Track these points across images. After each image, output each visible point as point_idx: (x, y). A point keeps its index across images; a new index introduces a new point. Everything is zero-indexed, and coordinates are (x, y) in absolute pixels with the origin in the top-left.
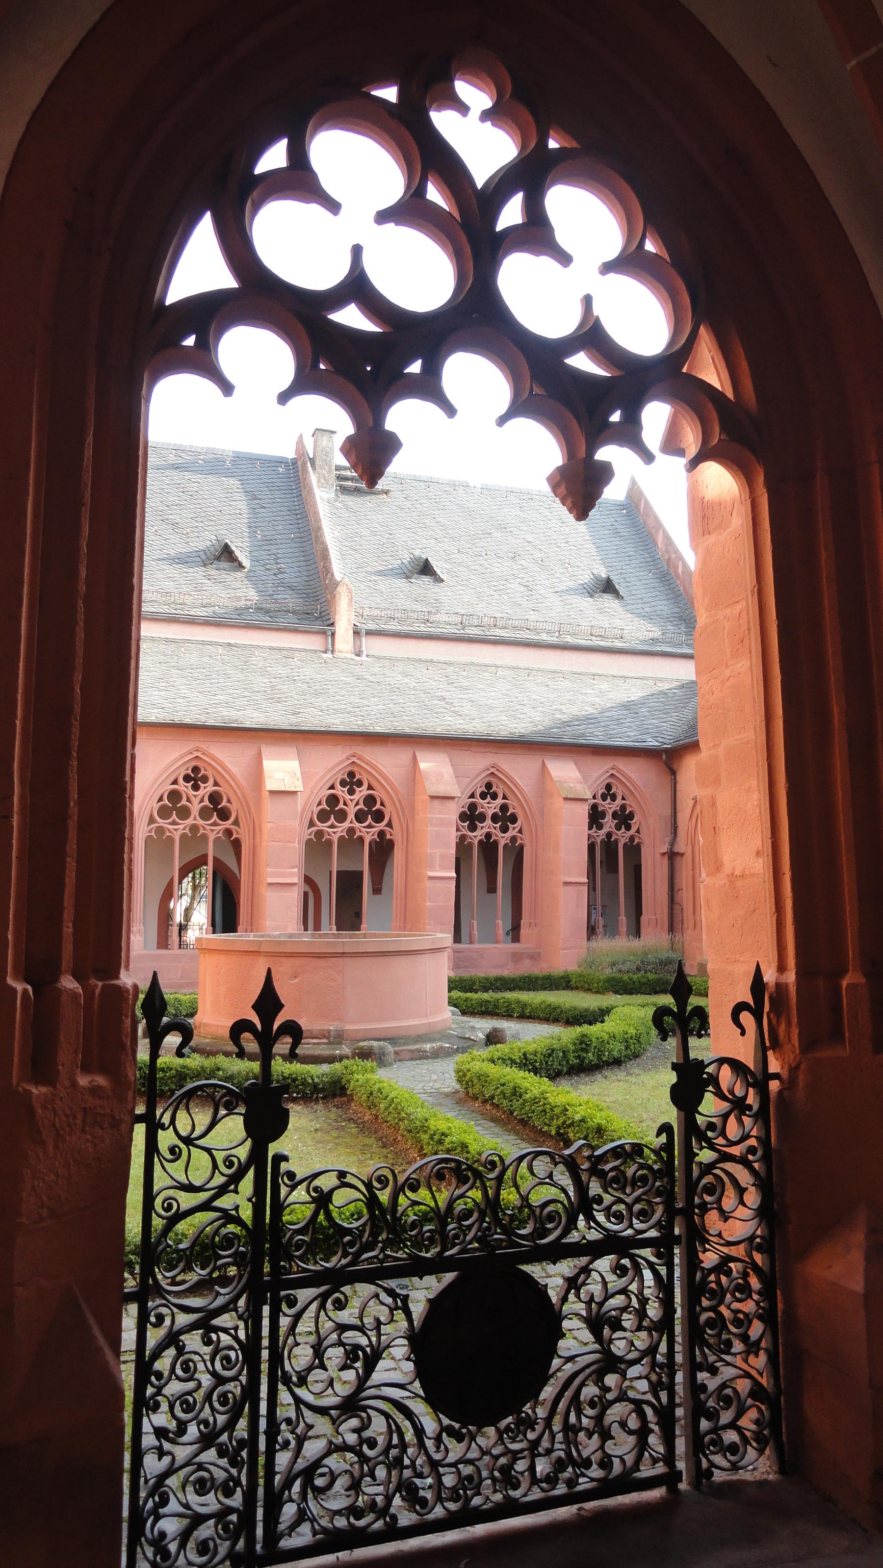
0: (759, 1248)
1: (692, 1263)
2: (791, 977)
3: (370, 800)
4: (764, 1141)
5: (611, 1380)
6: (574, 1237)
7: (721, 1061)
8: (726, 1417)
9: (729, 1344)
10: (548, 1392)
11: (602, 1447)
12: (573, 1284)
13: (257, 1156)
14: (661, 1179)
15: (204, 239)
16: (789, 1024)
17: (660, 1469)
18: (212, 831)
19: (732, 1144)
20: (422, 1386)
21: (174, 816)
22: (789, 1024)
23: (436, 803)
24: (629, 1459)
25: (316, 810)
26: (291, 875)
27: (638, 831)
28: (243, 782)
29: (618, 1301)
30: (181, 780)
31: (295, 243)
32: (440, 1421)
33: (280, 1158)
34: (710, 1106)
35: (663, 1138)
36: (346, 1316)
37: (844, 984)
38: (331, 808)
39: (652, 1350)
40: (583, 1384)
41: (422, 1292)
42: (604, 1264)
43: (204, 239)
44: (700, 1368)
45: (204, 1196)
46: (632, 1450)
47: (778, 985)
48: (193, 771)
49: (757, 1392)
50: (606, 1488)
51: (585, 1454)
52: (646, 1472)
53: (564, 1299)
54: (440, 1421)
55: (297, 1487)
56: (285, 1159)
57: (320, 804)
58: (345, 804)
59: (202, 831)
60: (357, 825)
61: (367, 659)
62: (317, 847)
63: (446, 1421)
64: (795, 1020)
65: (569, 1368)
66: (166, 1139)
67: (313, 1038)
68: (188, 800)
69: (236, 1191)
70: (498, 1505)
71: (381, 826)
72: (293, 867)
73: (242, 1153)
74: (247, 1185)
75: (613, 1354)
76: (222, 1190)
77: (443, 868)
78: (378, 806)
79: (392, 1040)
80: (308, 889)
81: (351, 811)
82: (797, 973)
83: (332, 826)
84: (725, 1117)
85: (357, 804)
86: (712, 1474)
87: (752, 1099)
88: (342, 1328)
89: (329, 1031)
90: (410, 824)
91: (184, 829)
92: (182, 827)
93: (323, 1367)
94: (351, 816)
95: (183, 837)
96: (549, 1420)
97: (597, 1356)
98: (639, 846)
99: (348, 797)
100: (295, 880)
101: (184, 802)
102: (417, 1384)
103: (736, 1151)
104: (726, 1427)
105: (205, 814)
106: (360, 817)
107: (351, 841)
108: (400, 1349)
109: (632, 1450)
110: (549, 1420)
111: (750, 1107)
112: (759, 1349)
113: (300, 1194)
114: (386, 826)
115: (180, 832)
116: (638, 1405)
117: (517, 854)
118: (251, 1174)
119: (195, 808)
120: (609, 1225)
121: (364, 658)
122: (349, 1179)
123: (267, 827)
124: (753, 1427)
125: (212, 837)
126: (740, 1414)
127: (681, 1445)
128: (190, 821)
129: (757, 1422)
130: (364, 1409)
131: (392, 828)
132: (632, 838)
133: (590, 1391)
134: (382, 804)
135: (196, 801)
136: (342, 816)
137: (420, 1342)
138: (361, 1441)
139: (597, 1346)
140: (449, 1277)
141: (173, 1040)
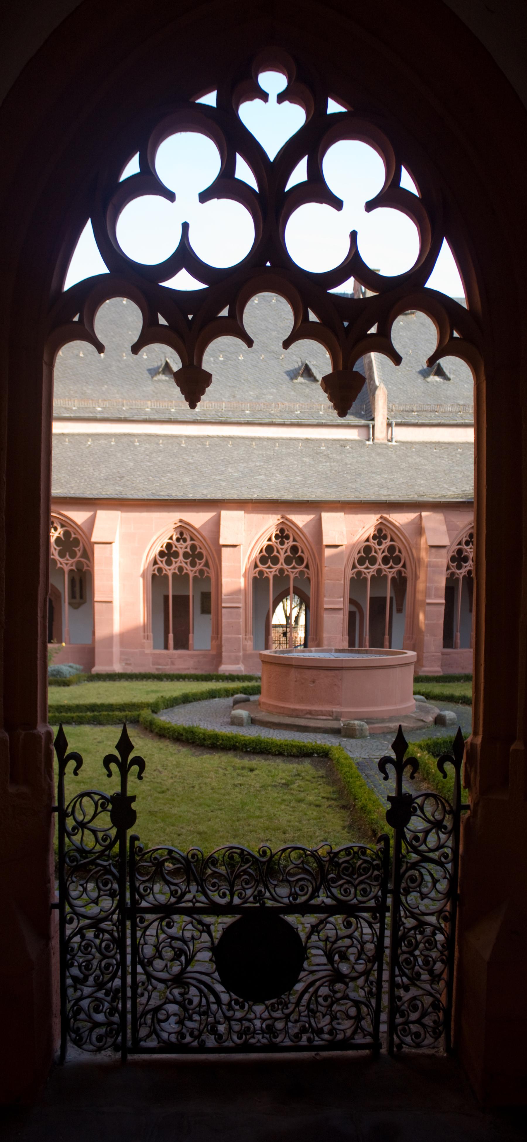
0: (445, 919)
1: (397, 923)
2: (479, 740)
3: (391, 549)
4: (455, 850)
5: (338, 986)
8: (414, 1016)
9: (419, 974)
10: (299, 987)
11: (330, 1023)
12: (315, 929)
13: (121, 835)
14: (378, 870)
16: (476, 772)
17: (368, 1040)
18: (293, 572)
19: (431, 850)
20: (219, 975)
21: (269, 563)
22: (476, 772)
23: (433, 550)
24: (349, 1033)
25: (357, 557)
26: (339, 602)
28: (310, 539)
29: (347, 942)
30: (273, 538)
31: (145, 231)
33: (134, 838)
34: (416, 823)
36: (173, 931)
37: (511, 749)
39: (366, 973)
40: (322, 985)
41: (219, 924)
42: (338, 919)
44: (399, 986)
46: (351, 1027)
47: (472, 744)
49: (436, 1005)
50: (332, 1045)
51: (320, 1026)
52: (359, 1039)
53: (309, 937)
56: (137, 839)
57: (359, 552)
58: (376, 552)
59: (286, 573)
60: (383, 567)
61: (395, 444)
62: (357, 582)
63: (234, 997)
64: (478, 771)
65: (311, 978)
66: (70, 823)
67: (322, 715)
68: (278, 552)
70: (264, 1045)
71: (399, 567)
72: (340, 598)
73: (113, 832)
77: (437, 596)
78: (397, 553)
79: (369, 721)
80: (354, 609)
81: (380, 557)
82: (483, 738)
84: (427, 832)
85: (383, 552)
86: (402, 1047)
87: (448, 823)
88: (173, 938)
89: (332, 712)
90: (417, 565)
91: (276, 571)
92: (273, 570)
93: (161, 957)
94: (380, 560)
95: (275, 576)
96: (298, 1003)
97: (330, 972)
99: (377, 547)
100: (341, 606)
101: (275, 553)
102: (216, 974)
103: (435, 855)
104: (413, 1022)
105: (288, 561)
107: (379, 578)
108: (206, 955)
109: (351, 1027)
110: (298, 1003)
111: (445, 827)
112: (439, 980)
115: (273, 573)
116: (357, 1004)
119: (282, 557)
120: (339, 896)
121: (394, 443)
122: (174, 854)
123: (325, 570)
124: (431, 1024)
125: (292, 576)
126: (423, 1015)
127: (383, 1028)
128: (279, 566)
129: (434, 1022)
130: (188, 984)
133: (324, 991)
134: (400, 552)
135: (282, 552)
136: (373, 561)
137: (218, 951)
138: (184, 1000)
139: (329, 967)
140: (238, 917)
141: (72, 764)
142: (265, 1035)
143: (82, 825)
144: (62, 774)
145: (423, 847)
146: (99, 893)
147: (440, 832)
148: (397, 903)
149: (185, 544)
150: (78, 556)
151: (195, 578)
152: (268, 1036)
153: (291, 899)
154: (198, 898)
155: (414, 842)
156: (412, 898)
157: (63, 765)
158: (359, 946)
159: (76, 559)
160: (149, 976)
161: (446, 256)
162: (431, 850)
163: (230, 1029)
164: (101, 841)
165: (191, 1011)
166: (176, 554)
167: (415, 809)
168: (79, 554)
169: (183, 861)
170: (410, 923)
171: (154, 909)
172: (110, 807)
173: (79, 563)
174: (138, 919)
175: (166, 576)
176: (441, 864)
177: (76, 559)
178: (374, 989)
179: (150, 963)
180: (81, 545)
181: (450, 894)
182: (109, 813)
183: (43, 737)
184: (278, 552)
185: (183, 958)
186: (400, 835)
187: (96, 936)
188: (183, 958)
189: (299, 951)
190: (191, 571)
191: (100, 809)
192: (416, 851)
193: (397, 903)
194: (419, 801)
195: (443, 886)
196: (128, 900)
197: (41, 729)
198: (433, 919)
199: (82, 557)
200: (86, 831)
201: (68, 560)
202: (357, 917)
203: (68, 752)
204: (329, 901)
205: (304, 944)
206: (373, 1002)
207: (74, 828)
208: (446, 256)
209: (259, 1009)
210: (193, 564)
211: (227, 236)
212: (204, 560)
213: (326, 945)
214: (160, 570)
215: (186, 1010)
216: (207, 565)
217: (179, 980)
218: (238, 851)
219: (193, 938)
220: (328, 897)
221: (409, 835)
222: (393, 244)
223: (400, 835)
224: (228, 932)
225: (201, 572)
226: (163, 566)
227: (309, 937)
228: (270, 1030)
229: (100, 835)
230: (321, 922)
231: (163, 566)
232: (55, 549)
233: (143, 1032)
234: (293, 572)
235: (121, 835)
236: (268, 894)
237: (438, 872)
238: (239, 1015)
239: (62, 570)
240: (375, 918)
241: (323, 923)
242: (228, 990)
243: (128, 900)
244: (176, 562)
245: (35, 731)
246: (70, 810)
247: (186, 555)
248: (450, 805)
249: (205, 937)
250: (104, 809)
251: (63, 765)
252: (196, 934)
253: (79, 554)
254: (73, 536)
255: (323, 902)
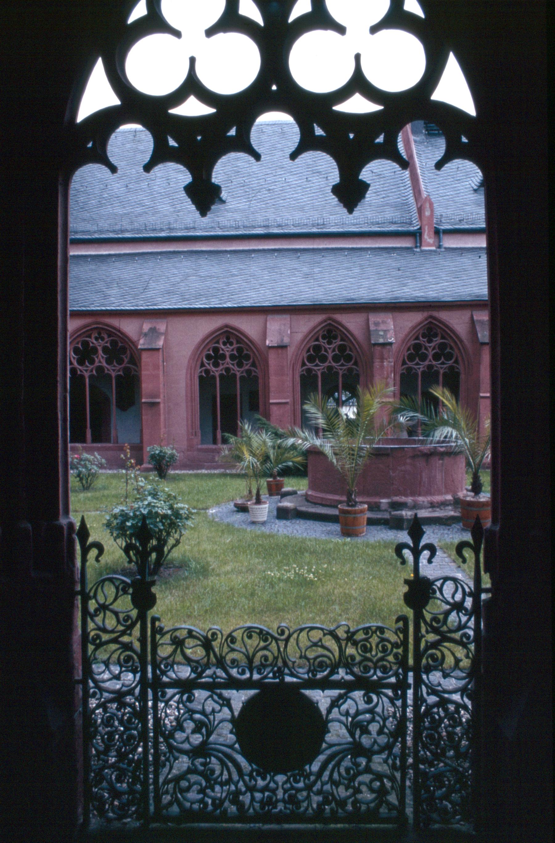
6: (335, 677)
7: (446, 579)
12: (335, 703)
15: (98, 74)
19: (450, 631)
31: (152, 66)
32: (252, 767)
33: (154, 620)
35: (401, 624)
39: (389, 747)
41: (239, 698)
42: (358, 694)
43: (98, 74)
45: (113, 636)
53: (329, 711)
54: (252, 767)
55: (171, 786)
56: (159, 619)
66: (92, 605)
69: (130, 635)
73: (134, 613)
74: (136, 631)
75: (281, 773)
76: (123, 633)
81: (431, 353)
94: (330, 358)
105: (336, 359)
111: (466, 610)
113: (167, 639)
116: (379, 777)
118: (138, 626)
119: (330, 355)
122: (194, 633)
136: (324, 359)
137: (239, 724)
141: (93, 553)
142: (288, 806)
143: (103, 608)
144: (84, 560)
145: (445, 628)
146: (121, 669)
147: (460, 614)
148: (418, 681)
149: (232, 347)
150: (125, 363)
151: (242, 377)
152: (291, 806)
153: (310, 675)
154: (218, 674)
155: (434, 624)
156: (435, 677)
157: (85, 551)
158: (382, 723)
159: (123, 366)
160: (171, 747)
161: (453, 68)
162: (450, 631)
163: (253, 799)
164: (122, 622)
165: (212, 782)
166: (223, 357)
167: (434, 592)
168: (126, 360)
169: (202, 639)
170: (432, 699)
171: (178, 683)
172: (131, 591)
173: (127, 370)
174: (160, 693)
175: (214, 377)
176: (464, 645)
177: (123, 366)
178: (398, 762)
179: (171, 735)
180: (128, 352)
181: (472, 673)
182: (130, 597)
183: (65, 527)
184: (326, 350)
185: (204, 730)
186: (419, 616)
187: (118, 709)
188: (204, 730)
189: (320, 725)
190: (238, 372)
191: (121, 593)
192: (436, 631)
193: (418, 681)
194: (438, 584)
195: (465, 663)
196: (150, 675)
197: (63, 521)
198: (456, 697)
199: (129, 363)
200: (108, 613)
201: (115, 366)
202: (378, 694)
203: (90, 540)
204: (349, 677)
205: (324, 717)
206: (398, 775)
207: (96, 610)
208: (453, 68)
209: (280, 778)
210: (240, 365)
211: (234, 66)
212: (251, 360)
213: (347, 719)
214: (207, 372)
215: (207, 780)
216: (254, 365)
217: (202, 751)
218: (258, 631)
219: (213, 711)
220: (347, 673)
221: (428, 617)
222: (398, 62)
223: (419, 616)
224: (248, 705)
225: (249, 372)
226: (211, 367)
227: (329, 711)
228: (292, 800)
229: (121, 616)
230: (340, 697)
231: (211, 367)
232: (103, 357)
233: (166, 799)
234: (341, 368)
235: (142, 617)
236: (286, 671)
237: (460, 652)
238: (261, 783)
239: (110, 376)
240: (396, 694)
241: (343, 698)
242: (250, 761)
243: (150, 675)
244: (223, 364)
245: (57, 522)
246: (92, 594)
247: (232, 357)
248: (469, 588)
249: (226, 710)
250: (125, 592)
251: (85, 551)
252: (217, 707)
253: (126, 360)
254: (120, 344)
255: (343, 678)
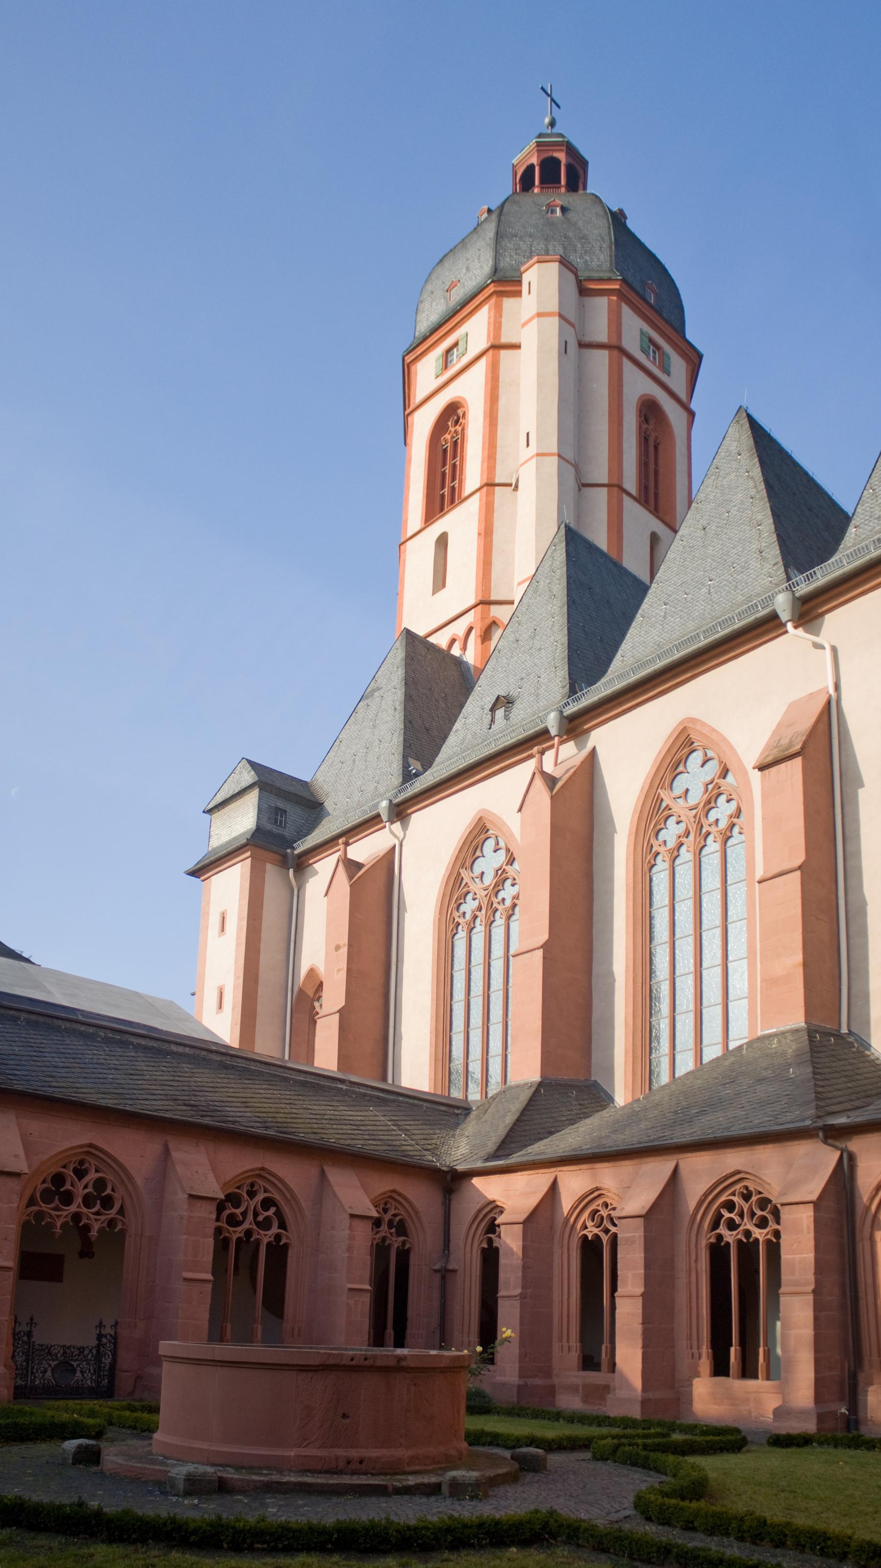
27: (121, 1211)
38: (56, 1188)
48: (79, 1164)
57: (44, 1182)
83: (56, 1209)
91: (65, 1217)
98: (286, 1247)
106: (88, 1201)
114: (117, 1213)
117: (279, 1253)
131: (124, 1217)
132: (111, 1223)
